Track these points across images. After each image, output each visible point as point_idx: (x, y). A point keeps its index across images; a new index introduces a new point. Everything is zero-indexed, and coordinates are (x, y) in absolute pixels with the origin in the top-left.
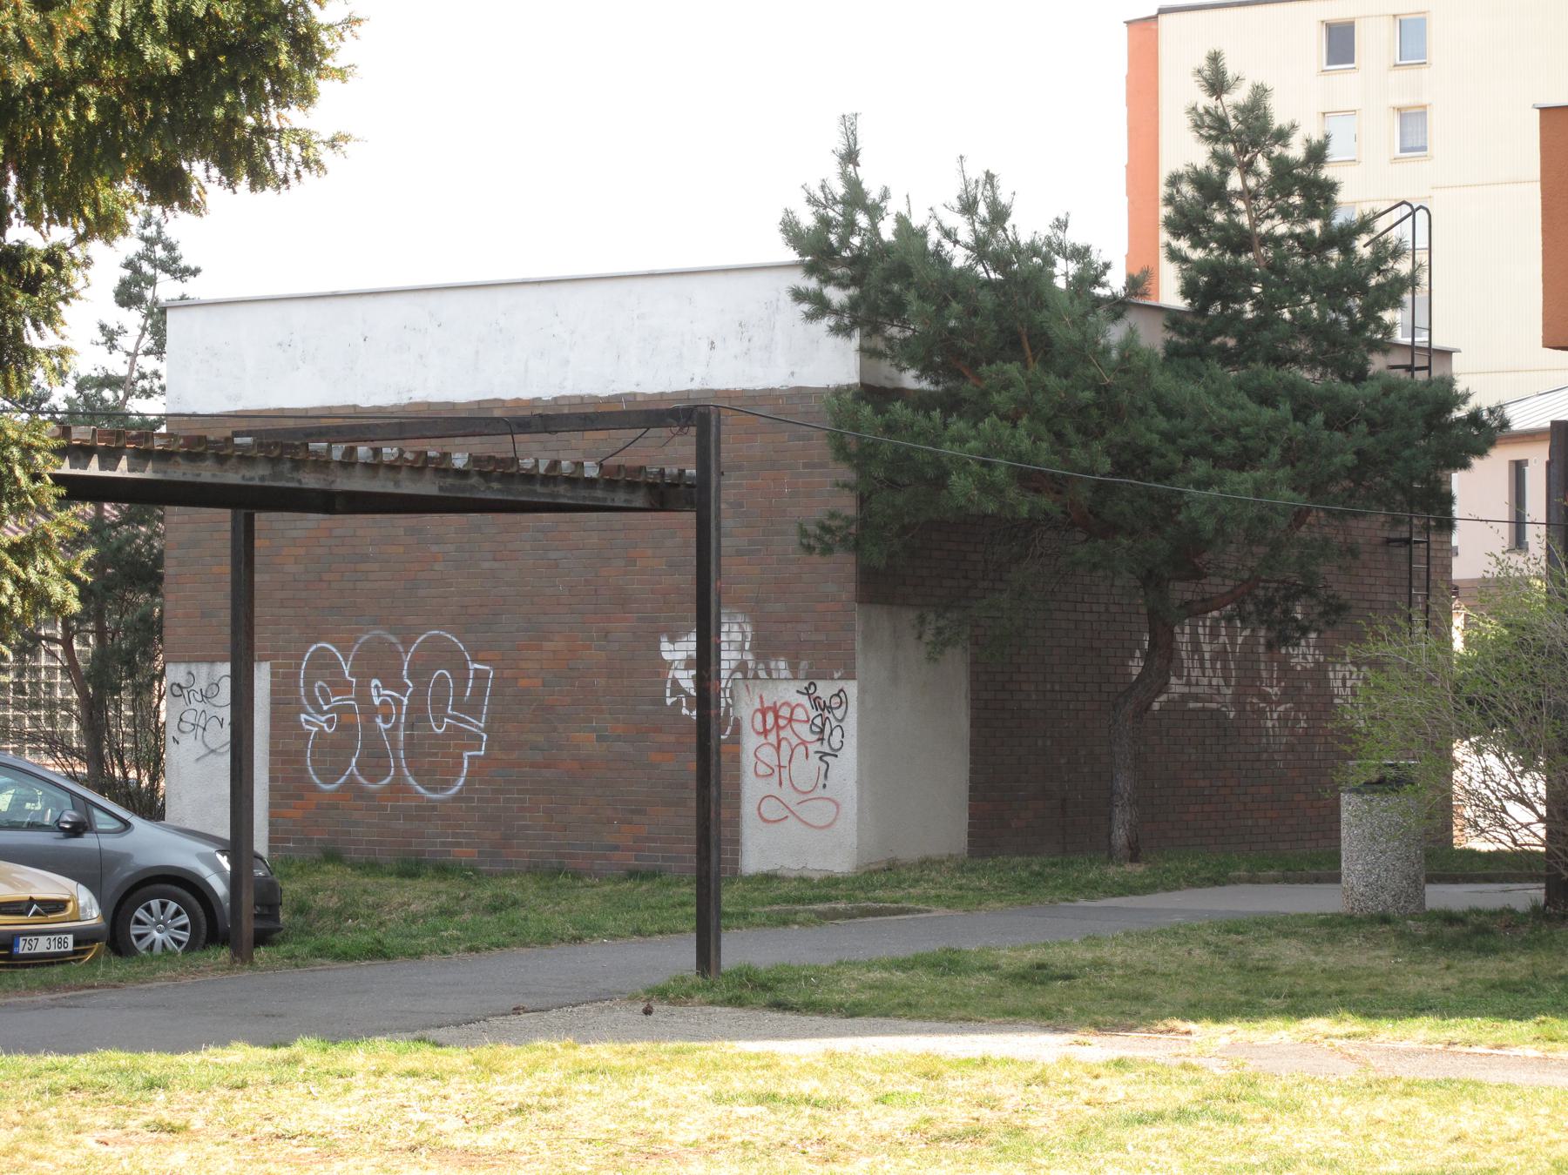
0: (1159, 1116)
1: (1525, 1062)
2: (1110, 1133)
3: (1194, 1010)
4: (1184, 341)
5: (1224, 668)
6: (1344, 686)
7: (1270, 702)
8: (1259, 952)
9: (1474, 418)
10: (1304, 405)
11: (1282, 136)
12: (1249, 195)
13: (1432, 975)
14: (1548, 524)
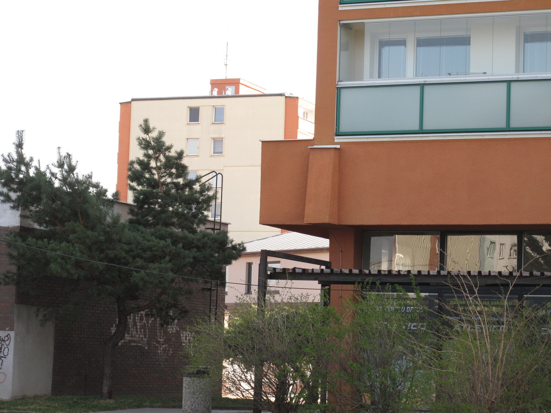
5: (145, 331)
6: (186, 339)
10: (175, 241)
11: (169, 148)
14: (259, 286)
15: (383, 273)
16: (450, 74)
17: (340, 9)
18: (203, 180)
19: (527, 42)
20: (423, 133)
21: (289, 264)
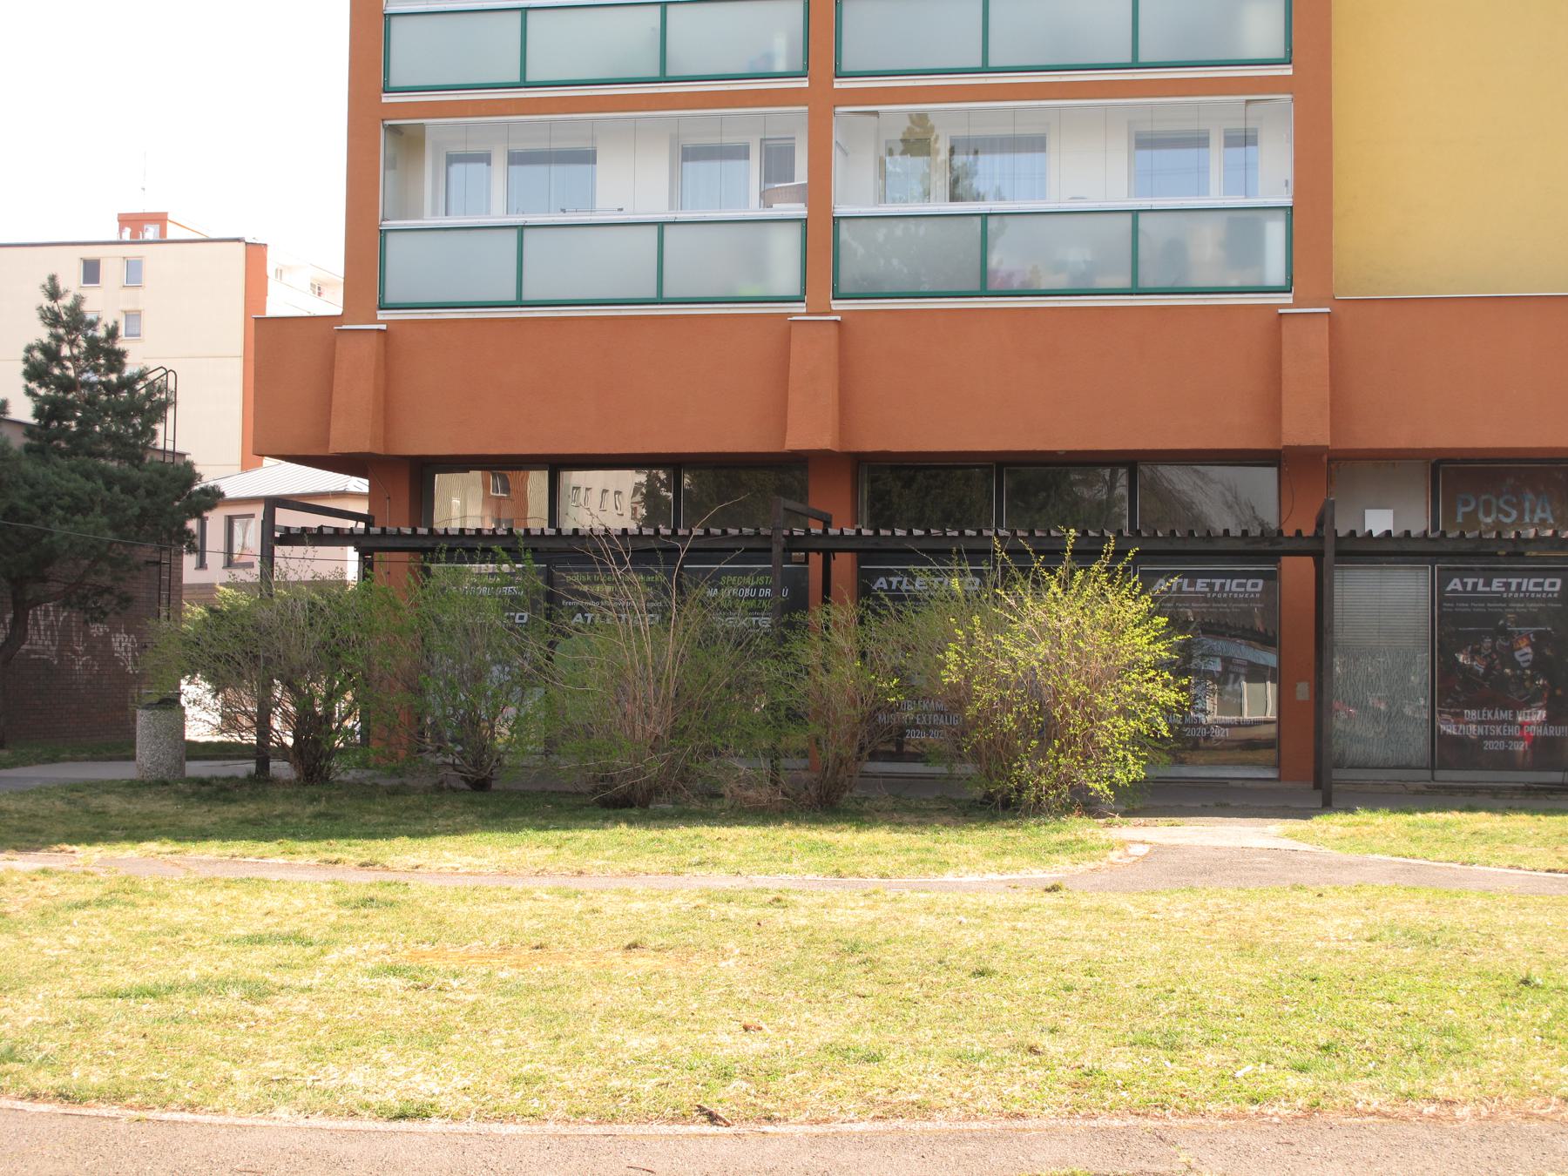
0: (87, 904)
1: (279, 866)
2: (60, 914)
3: (74, 838)
4: (35, 443)
5: (52, 635)
6: (120, 646)
7: (77, 655)
8: (95, 803)
9: (204, 491)
10: (110, 480)
11: (92, 325)
12: (74, 359)
13: (199, 816)
14: (262, 556)
15: (467, 533)
16: (564, 211)
17: (384, 100)
18: (152, 377)
19: (687, 161)
20: (522, 306)
21: (313, 521)
